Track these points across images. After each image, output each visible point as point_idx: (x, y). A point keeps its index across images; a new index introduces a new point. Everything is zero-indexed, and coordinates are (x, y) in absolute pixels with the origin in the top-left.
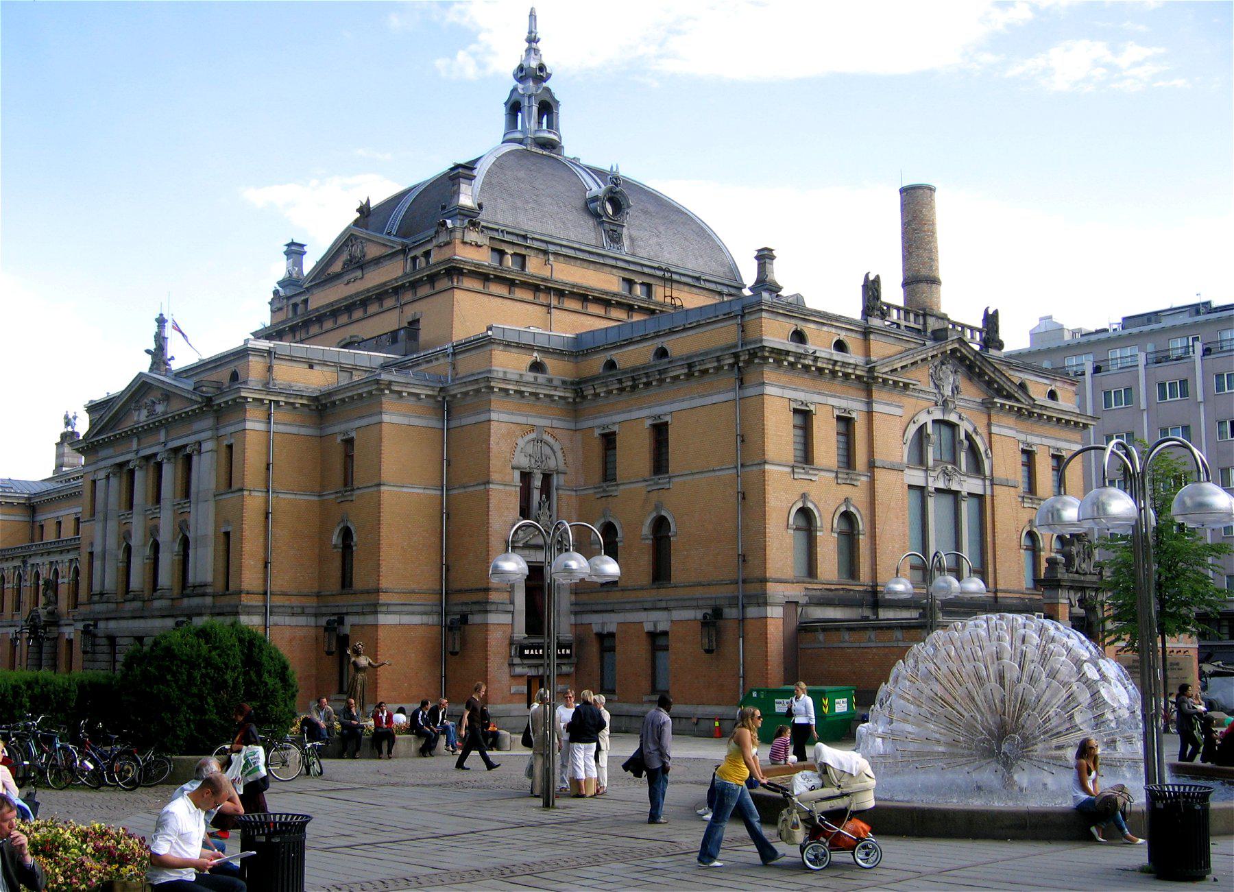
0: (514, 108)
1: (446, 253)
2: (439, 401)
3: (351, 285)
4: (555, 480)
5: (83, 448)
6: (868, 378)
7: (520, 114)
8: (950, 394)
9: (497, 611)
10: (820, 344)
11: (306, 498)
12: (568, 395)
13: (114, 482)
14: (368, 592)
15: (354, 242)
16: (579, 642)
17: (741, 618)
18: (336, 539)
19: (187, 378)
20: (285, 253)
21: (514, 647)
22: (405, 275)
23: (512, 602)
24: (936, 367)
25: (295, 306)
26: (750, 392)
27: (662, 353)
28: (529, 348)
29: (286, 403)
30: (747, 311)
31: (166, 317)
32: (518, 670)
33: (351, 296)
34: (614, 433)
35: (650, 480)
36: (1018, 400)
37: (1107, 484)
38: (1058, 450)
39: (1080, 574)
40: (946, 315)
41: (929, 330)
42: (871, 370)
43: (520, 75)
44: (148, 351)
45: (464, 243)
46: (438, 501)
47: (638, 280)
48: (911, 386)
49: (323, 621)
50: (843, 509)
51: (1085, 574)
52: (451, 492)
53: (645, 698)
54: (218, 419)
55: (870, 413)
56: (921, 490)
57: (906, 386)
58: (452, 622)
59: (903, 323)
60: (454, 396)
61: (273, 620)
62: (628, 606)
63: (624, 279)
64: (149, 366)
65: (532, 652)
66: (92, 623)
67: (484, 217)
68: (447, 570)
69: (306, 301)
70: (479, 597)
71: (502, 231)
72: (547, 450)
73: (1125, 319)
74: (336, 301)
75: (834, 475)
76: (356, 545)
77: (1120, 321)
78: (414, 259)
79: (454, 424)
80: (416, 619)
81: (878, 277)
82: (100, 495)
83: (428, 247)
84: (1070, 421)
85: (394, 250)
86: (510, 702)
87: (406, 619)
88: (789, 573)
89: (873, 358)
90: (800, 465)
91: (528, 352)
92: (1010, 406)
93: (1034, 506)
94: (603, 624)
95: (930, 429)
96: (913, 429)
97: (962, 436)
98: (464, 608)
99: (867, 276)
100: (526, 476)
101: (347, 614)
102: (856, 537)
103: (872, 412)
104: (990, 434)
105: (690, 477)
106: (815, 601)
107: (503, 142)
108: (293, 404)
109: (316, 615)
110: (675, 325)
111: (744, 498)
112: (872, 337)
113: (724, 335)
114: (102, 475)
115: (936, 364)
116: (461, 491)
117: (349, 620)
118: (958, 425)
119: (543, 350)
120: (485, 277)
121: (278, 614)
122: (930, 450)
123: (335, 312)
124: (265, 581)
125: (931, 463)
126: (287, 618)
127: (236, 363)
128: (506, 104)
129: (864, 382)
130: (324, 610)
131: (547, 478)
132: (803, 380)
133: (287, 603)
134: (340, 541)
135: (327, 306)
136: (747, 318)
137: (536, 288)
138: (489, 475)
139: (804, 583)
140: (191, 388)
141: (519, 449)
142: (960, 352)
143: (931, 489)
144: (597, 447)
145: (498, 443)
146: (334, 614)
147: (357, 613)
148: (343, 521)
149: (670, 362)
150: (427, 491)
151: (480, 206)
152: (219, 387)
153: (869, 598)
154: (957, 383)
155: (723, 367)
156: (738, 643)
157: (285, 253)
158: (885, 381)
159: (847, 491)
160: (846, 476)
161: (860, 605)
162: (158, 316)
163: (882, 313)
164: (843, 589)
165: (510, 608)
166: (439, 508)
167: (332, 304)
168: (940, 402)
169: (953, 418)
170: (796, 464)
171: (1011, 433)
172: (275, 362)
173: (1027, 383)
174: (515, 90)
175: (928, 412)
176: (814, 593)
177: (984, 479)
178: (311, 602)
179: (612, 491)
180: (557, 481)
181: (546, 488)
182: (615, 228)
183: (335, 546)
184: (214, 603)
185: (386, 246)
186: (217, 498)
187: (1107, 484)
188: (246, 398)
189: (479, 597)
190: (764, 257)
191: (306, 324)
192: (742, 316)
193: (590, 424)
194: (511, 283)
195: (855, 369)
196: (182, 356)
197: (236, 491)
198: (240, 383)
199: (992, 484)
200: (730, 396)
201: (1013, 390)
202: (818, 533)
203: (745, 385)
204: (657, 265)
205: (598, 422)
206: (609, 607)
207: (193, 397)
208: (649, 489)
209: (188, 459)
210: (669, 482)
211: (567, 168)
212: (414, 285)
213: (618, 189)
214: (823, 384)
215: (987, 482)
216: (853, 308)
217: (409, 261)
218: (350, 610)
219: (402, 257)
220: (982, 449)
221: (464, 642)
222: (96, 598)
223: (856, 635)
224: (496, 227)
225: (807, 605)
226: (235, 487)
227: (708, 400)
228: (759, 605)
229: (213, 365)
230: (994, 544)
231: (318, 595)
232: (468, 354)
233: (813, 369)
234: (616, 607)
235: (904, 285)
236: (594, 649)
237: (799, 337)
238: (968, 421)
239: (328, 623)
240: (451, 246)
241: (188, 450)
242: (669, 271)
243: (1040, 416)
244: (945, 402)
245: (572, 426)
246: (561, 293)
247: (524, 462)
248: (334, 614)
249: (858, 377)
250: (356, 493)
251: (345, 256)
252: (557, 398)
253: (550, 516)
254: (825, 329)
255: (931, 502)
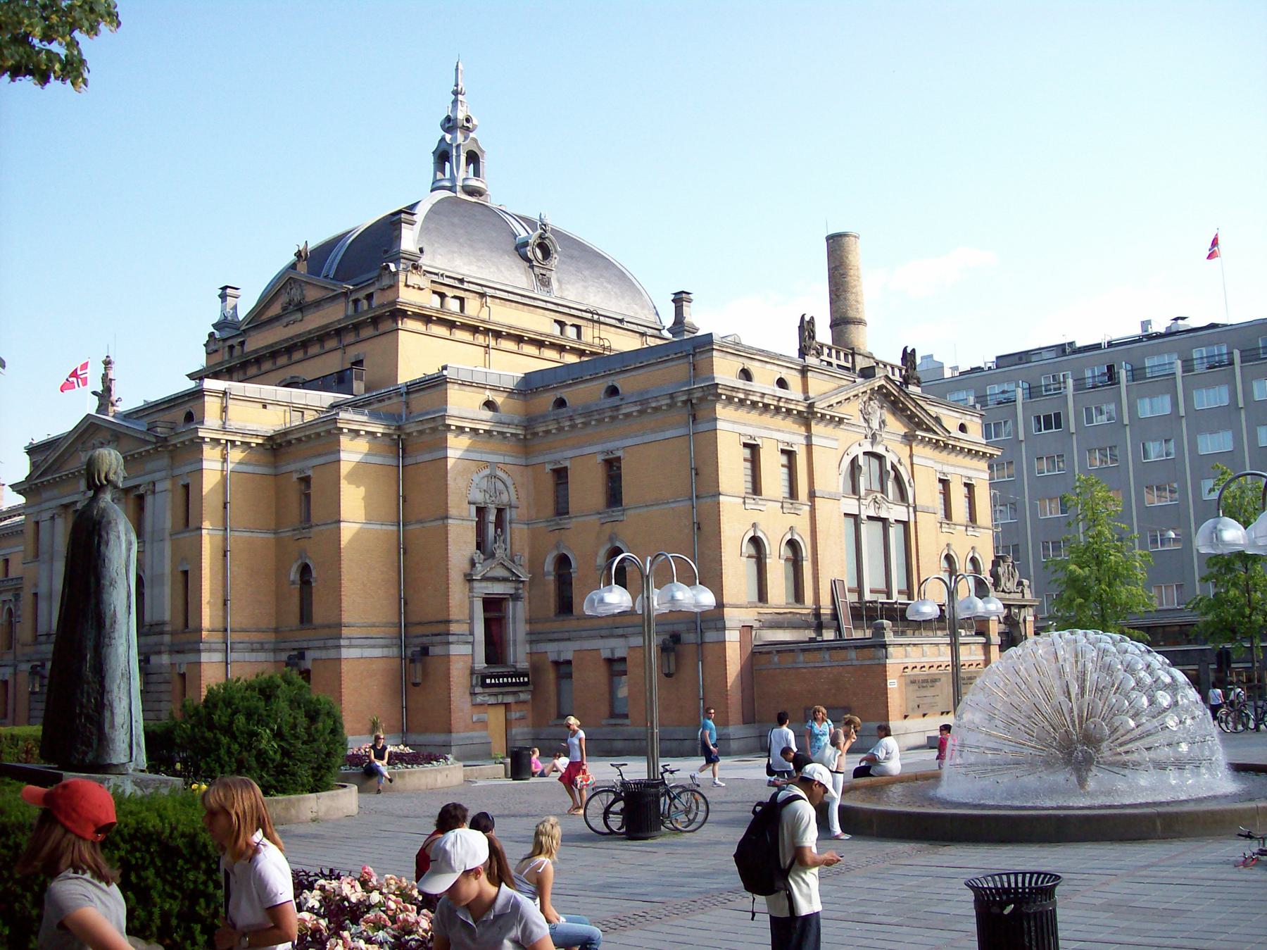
0: (443, 156)
1: (389, 296)
2: (394, 439)
3: (290, 327)
4: (508, 515)
5: (25, 489)
6: (808, 413)
7: (447, 165)
8: (878, 427)
9: (458, 643)
10: (764, 382)
11: (262, 535)
12: (519, 432)
13: (60, 522)
14: (329, 627)
15: (293, 285)
16: (536, 669)
17: (700, 642)
18: (294, 575)
19: (137, 418)
20: (219, 296)
21: (475, 677)
22: (347, 317)
23: (472, 633)
24: (865, 402)
25: (231, 347)
26: (702, 427)
27: (613, 391)
28: (483, 387)
29: (242, 442)
30: (698, 350)
31: (112, 359)
32: (479, 699)
33: (291, 338)
34: (565, 469)
35: (605, 513)
36: (935, 433)
37: (1221, 515)
38: (969, 478)
39: (1005, 592)
40: (871, 354)
41: (858, 368)
42: (811, 406)
43: (447, 125)
44: (94, 393)
45: (407, 286)
46: (395, 536)
47: (569, 321)
48: (845, 421)
49: (284, 656)
50: (788, 537)
51: (1010, 593)
52: (407, 528)
53: (604, 722)
54: (172, 458)
55: (809, 446)
56: (856, 518)
57: (841, 420)
58: (413, 655)
59: (834, 361)
60: (409, 434)
61: (233, 656)
62: (585, 634)
63: (556, 321)
64: (96, 407)
65: (505, 680)
66: (39, 663)
67: (424, 261)
68: (406, 603)
69: (242, 344)
70: (441, 628)
71: (442, 275)
72: (500, 485)
73: (998, 358)
74: (276, 343)
75: (742, 500)
76: (316, 581)
77: (994, 360)
78: (356, 302)
79: (409, 461)
80: (378, 652)
81: (812, 318)
82: (44, 535)
83: (371, 290)
84: (979, 451)
85: (335, 293)
86: (473, 730)
87: (368, 652)
88: (744, 600)
89: (811, 394)
90: (751, 496)
91: (482, 390)
92: (929, 438)
93: (951, 531)
94: (559, 652)
95: (861, 461)
96: (847, 461)
97: (889, 467)
98: (425, 640)
99: (803, 317)
100: (481, 511)
101: (308, 649)
102: (800, 563)
103: (812, 445)
104: (912, 464)
105: (645, 509)
106: (767, 625)
107: (432, 191)
108: (249, 443)
109: (275, 651)
110: (625, 364)
111: (699, 528)
112: (809, 374)
113: (673, 374)
114: (46, 516)
115: (864, 400)
116: (418, 526)
117: (310, 655)
118: (884, 457)
119: (495, 389)
120: (427, 320)
121: (239, 651)
122: (862, 480)
123: (274, 353)
124: (225, 618)
125: (863, 492)
126: (246, 654)
127: (191, 404)
128: (433, 153)
129: (805, 417)
130: (283, 645)
131: (500, 511)
132: (754, 416)
133: (247, 639)
134: (298, 577)
135: (267, 347)
136: (698, 357)
137: (474, 330)
138: (447, 510)
139: (756, 607)
140: (145, 429)
141: (474, 485)
142: (886, 388)
143: (863, 516)
144: (549, 482)
145: (455, 479)
146: (294, 649)
147: (319, 648)
148: (301, 557)
149: (622, 399)
150: (384, 527)
151: (421, 250)
152: (173, 427)
153: (811, 619)
154: (883, 418)
155: (676, 404)
156: (698, 666)
157: (219, 296)
158: (823, 415)
159: (791, 520)
160: (791, 506)
161: (807, 626)
162: (104, 358)
163: (818, 353)
164: (790, 613)
165: (470, 639)
166: (396, 543)
167: (271, 346)
168: (870, 435)
169: (879, 449)
170: (747, 496)
171: (930, 463)
172: (230, 402)
173: (942, 417)
174: (443, 139)
175: (860, 445)
176: (766, 617)
177: (908, 507)
178: (271, 637)
179: (565, 524)
180: (511, 516)
181: (499, 523)
182: (544, 272)
183: (293, 583)
184: (172, 641)
185: (326, 288)
186: (174, 537)
187: (1221, 515)
188: (203, 438)
189: (441, 628)
190: (680, 299)
191: (244, 365)
192: (694, 355)
193: (540, 459)
194: (451, 325)
195: (779, 401)
196: (129, 398)
197: (193, 531)
198: (197, 423)
199: (915, 511)
200: (682, 431)
201: (931, 423)
202: (768, 560)
203: (698, 421)
204: (584, 308)
205: (548, 458)
206: (566, 635)
207: (147, 438)
208: (603, 521)
209: (141, 498)
210: (623, 514)
211: (495, 217)
212: (357, 327)
213: (546, 235)
214: (766, 418)
215: (911, 509)
216: (791, 347)
217: (351, 303)
218: (311, 644)
219: (343, 299)
220: (906, 478)
221: (425, 674)
222: (43, 639)
223: (810, 656)
224: (436, 271)
225: (760, 628)
226: (192, 525)
227: (660, 436)
228: (717, 629)
229: (166, 406)
230: (918, 567)
231: (276, 630)
232: (422, 393)
233: (760, 405)
234: (573, 634)
235: (831, 327)
236: (551, 675)
237: (746, 375)
238: (894, 450)
239: (290, 658)
240: (394, 289)
241: (142, 490)
242: (597, 314)
243: (954, 447)
244: (874, 436)
245: (522, 461)
246: (498, 335)
247: (479, 497)
248: (294, 649)
249: (799, 412)
250: (315, 529)
251: (284, 299)
252: (509, 435)
253: (506, 550)
254: (768, 366)
255: (863, 528)
